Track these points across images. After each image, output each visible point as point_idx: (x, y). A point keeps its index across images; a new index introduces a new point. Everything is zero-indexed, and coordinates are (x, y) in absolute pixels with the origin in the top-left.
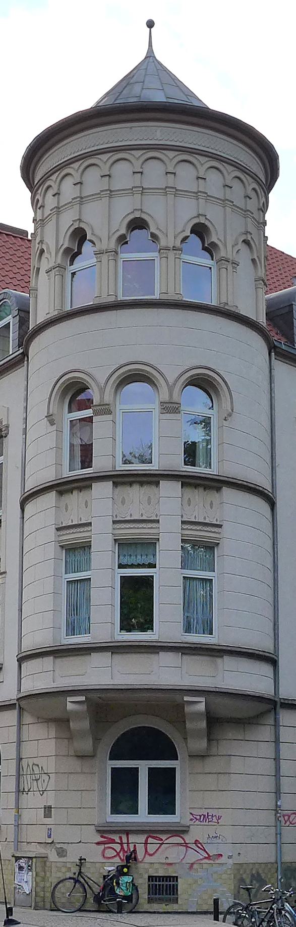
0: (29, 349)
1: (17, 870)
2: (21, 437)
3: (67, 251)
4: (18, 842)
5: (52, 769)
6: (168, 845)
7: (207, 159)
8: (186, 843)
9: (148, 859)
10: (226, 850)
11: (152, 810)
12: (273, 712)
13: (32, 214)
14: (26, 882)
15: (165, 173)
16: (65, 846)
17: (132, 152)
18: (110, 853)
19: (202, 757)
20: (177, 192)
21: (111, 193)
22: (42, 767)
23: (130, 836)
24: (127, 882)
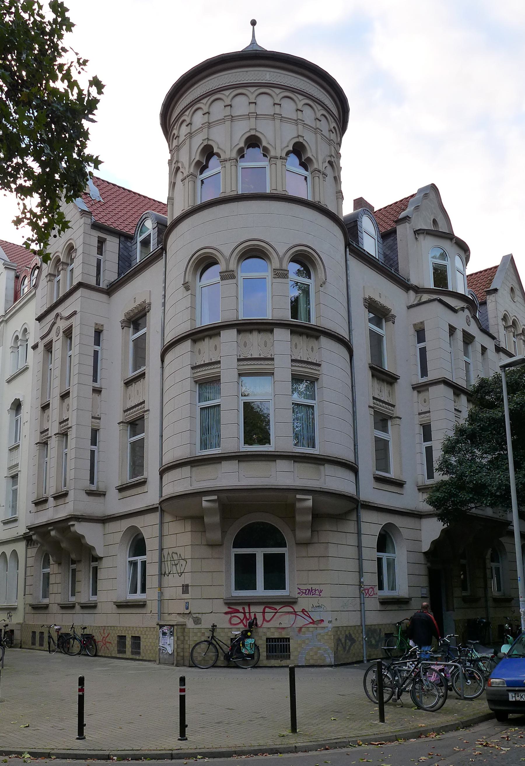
0: (167, 242)
1: (161, 635)
3: (198, 163)
4: (161, 614)
5: (188, 555)
6: (282, 613)
7: (303, 97)
8: (295, 612)
9: (266, 625)
10: (327, 617)
11: (267, 587)
12: (355, 510)
13: (169, 157)
14: (169, 644)
15: (273, 104)
16: (199, 616)
17: (250, 89)
18: (235, 620)
19: (307, 544)
20: (282, 119)
21: (232, 118)
22: (180, 555)
23: (251, 607)
24: (251, 643)
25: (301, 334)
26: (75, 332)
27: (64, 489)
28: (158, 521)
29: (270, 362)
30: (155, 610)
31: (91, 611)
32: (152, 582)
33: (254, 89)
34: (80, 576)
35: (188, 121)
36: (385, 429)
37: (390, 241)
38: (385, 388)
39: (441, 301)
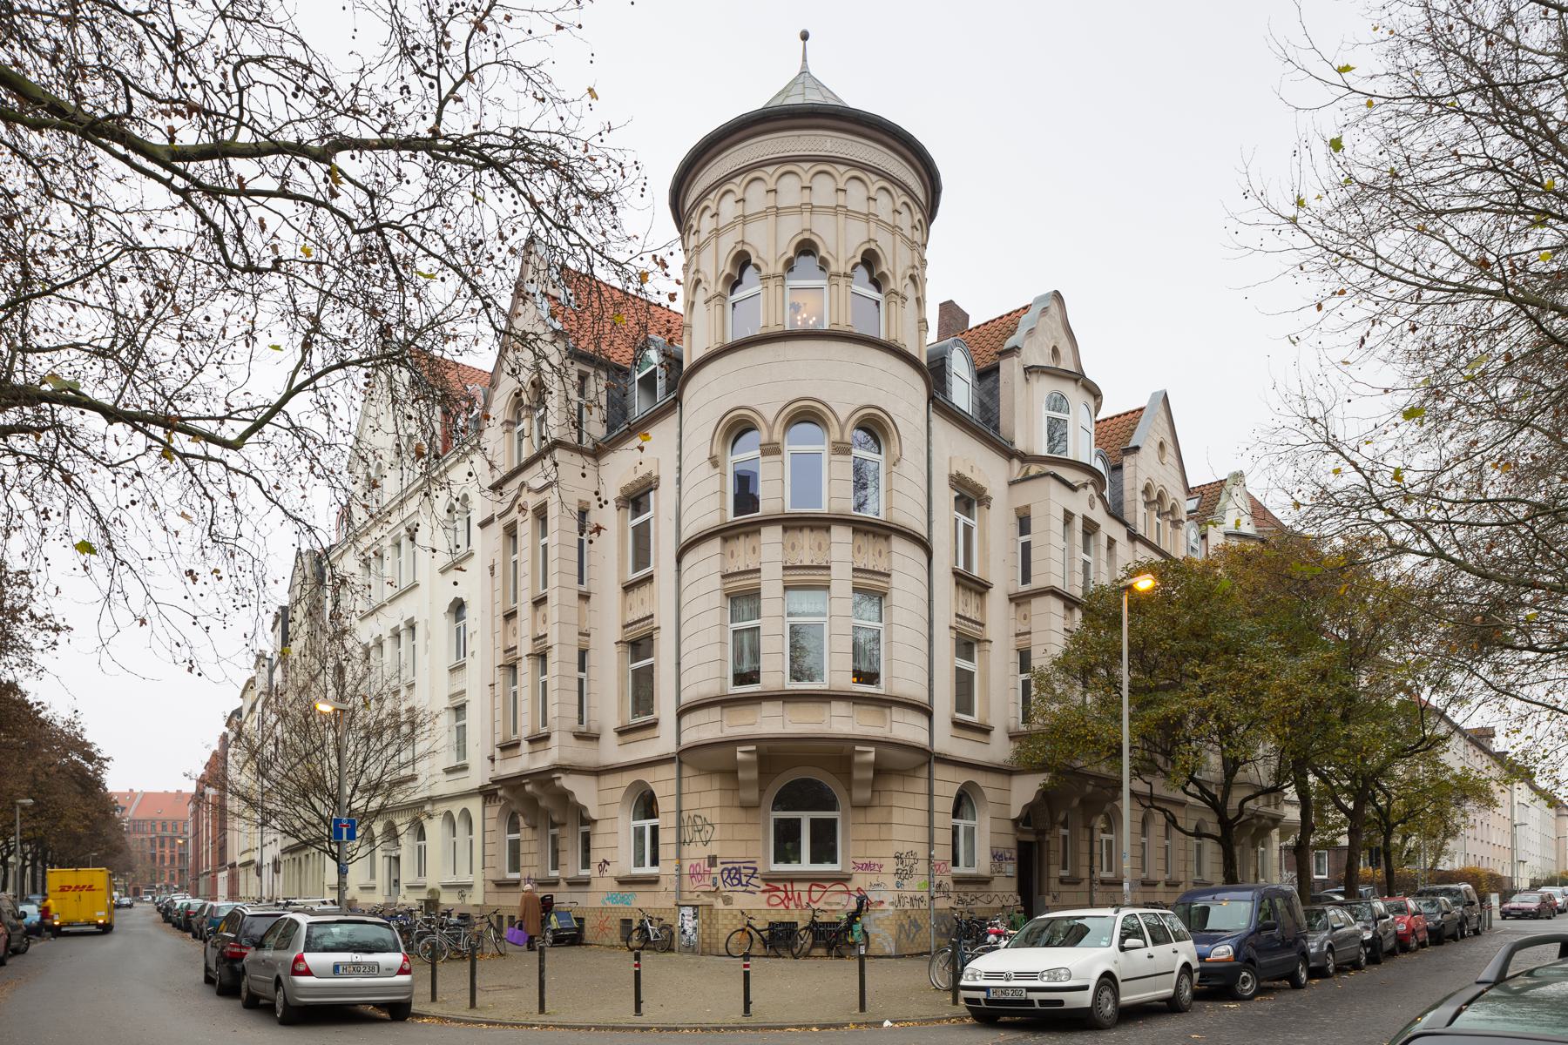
2: (675, 487)
3: (729, 277)
4: (680, 891)
11: (814, 860)
17: (801, 164)
18: (775, 901)
19: (864, 806)
25: (866, 533)
26: (553, 512)
27: (544, 730)
28: (674, 775)
29: (825, 572)
30: (672, 888)
31: (582, 889)
32: (667, 851)
33: (810, 165)
34: (564, 844)
35: (714, 211)
36: (969, 657)
37: (988, 382)
38: (974, 600)
39: (1055, 477)
